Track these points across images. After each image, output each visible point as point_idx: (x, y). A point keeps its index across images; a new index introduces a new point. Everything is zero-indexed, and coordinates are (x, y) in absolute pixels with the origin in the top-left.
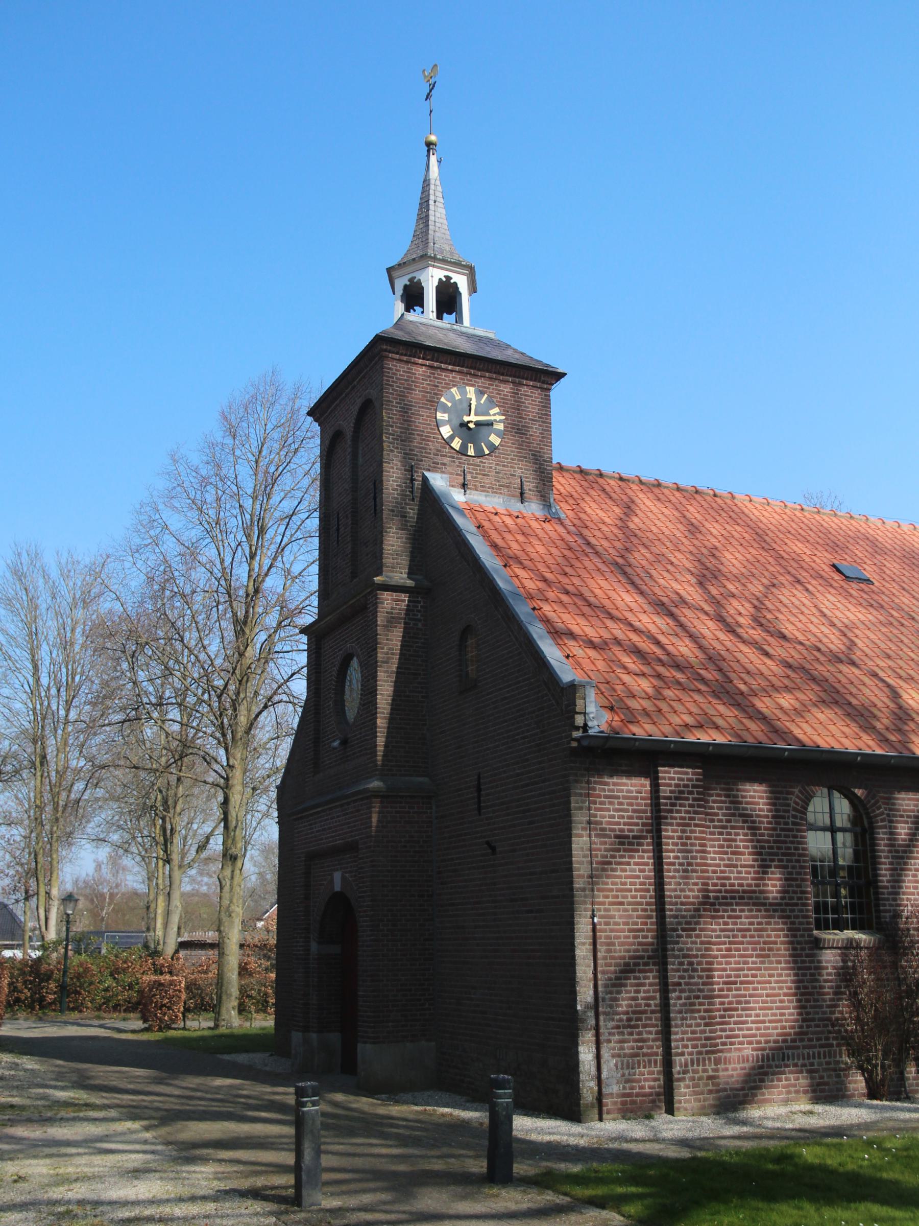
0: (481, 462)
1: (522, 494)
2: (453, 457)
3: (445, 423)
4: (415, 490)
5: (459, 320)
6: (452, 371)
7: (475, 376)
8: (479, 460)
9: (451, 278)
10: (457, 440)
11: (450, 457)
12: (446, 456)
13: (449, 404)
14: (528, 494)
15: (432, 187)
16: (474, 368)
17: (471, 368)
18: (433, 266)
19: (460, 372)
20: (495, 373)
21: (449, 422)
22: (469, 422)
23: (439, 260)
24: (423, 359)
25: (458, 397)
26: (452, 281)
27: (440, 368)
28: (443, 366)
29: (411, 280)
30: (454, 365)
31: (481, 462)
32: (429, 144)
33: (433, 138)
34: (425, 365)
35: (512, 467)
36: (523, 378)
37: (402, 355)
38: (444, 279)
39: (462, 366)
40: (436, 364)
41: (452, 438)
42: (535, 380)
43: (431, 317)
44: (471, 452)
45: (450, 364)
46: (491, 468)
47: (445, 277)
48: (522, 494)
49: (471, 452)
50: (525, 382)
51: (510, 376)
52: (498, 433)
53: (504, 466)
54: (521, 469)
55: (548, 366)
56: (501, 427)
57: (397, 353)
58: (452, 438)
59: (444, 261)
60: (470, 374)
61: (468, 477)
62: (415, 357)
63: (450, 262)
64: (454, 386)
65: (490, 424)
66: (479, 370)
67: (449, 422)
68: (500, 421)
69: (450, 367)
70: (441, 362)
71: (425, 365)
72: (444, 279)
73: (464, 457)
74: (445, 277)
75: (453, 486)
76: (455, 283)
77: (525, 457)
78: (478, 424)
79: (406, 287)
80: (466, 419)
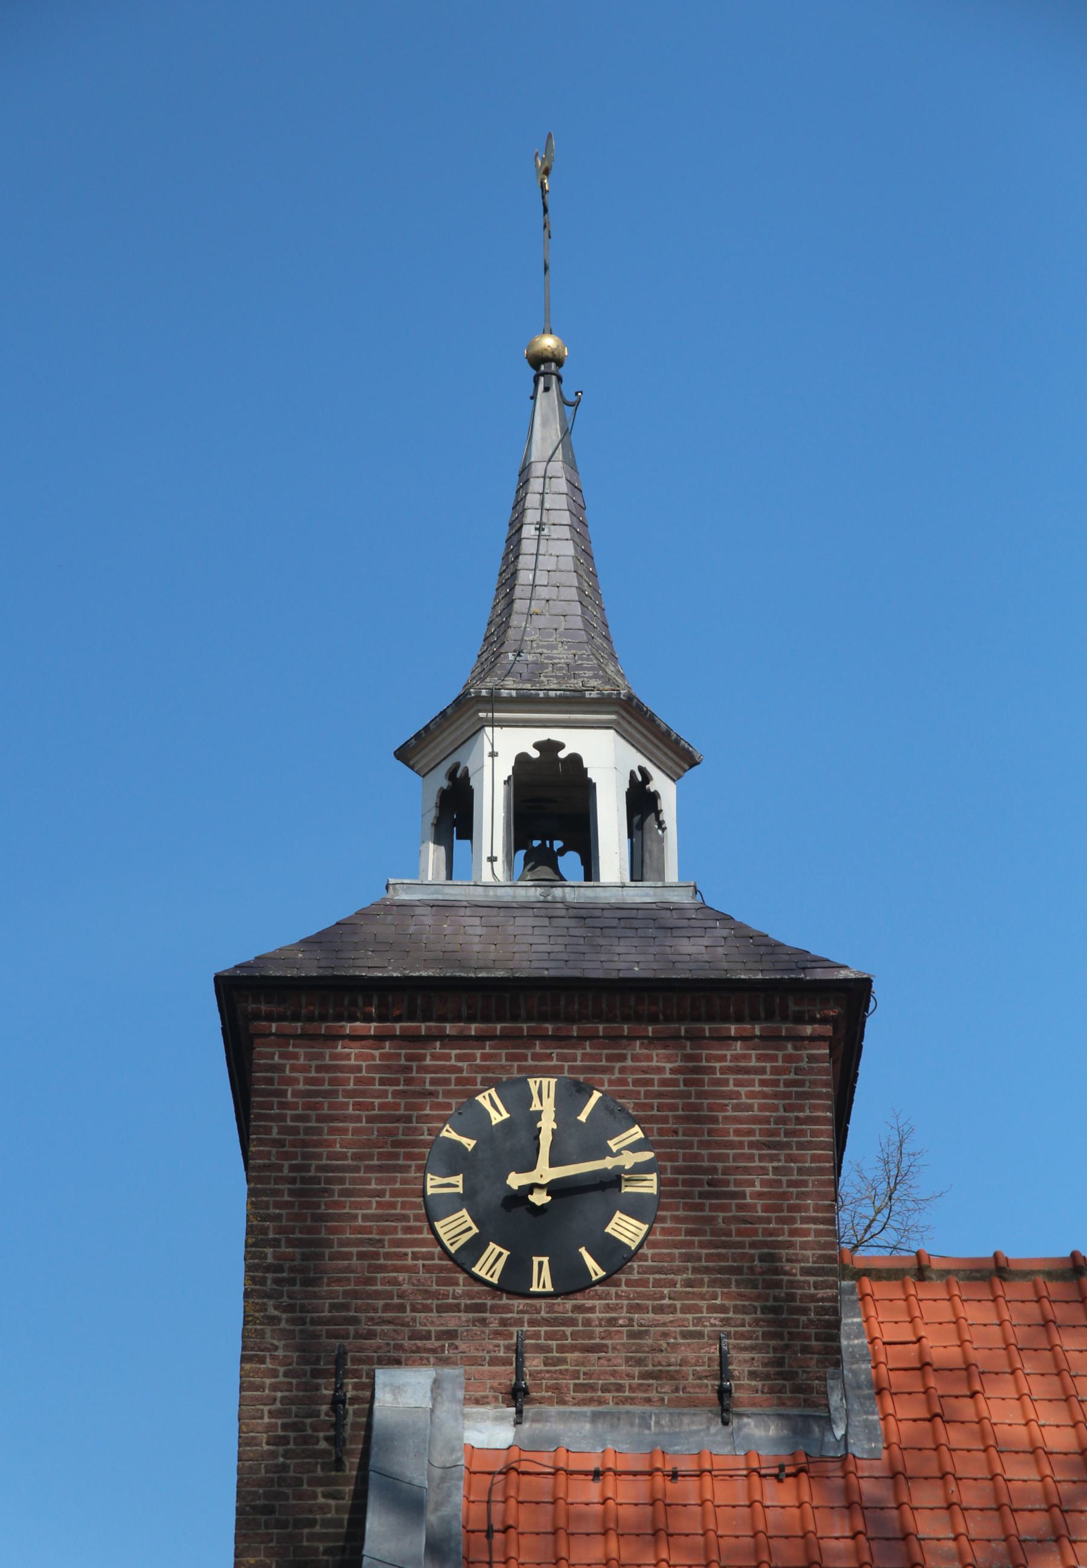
0: (578, 1309)
1: (723, 1393)
2: (480, 1308)
3: (452, 1204)
4: (348, 1432)
5: (590, 871)
6: (480, 1039)
7: (561, 1039)
8: (569, 1304)
9: (561, 746)
10: (494, 1249)
11: (469, 1309)
12: (456, 1308)
13: (469, 1143)
14: (744, 1388)
15: (536, 485)
16: (554, 1018)
17: (543, 1018)
18: (494, 723)
19: (506, 1038)
20: (626, 1019)
21: (466, 1200)
22: (531, 1188)
23: (510, 700)
24: (381, 1018)
25: (498, 1116)
26: (562, 754)
27: (443, 1038)
28: (449, 1028)
29: (452, 774)
30: (486, 1019)
31: (578, 1309)
32: (537, 361)
33: (549, 342)
34: (392, 1037)
35: (686, 1309)
36: (726, 1019)
37: (310, 1019)
38: (535, 754)
39: (515, 1018)
40: (423, 1027)
41: (475, 1248)
42: (769, 1017)
43: (487, 877)
44: (542, 1279)
45: (471, 1019)
46: (612, 1322)
47: (537, 746)
48: (723, 1393)
49: (542, 1279)
50: (733, 1029)
51: (681, 1019)
52: (636, 1208)
53: (658, 1310)
54: (723, 1309)
55: (804, 959)
56: (649, 1185)
57: (296, 1018)
58: (475, 1248)
59: (525, 701)
60: (544, 1038)
61: (534, 1363)
62: (352, 1018)
63: (548, 700)
64: (488, 1083)
65: (611, 1181)
66: (571, 1019)
67: (466, 1200)
68: (641, 1168)
69: (473, 1029)
70: (443, 1019)
71: (392, 1037)
72: (535, 754)
73: (519, 1303)
74: (537, 746)
75: (478, 1402)
76: (575, 760)
77: (738, 1271)
78: (555, 1188)
79: (522, 760)
80: (515, 1180)
